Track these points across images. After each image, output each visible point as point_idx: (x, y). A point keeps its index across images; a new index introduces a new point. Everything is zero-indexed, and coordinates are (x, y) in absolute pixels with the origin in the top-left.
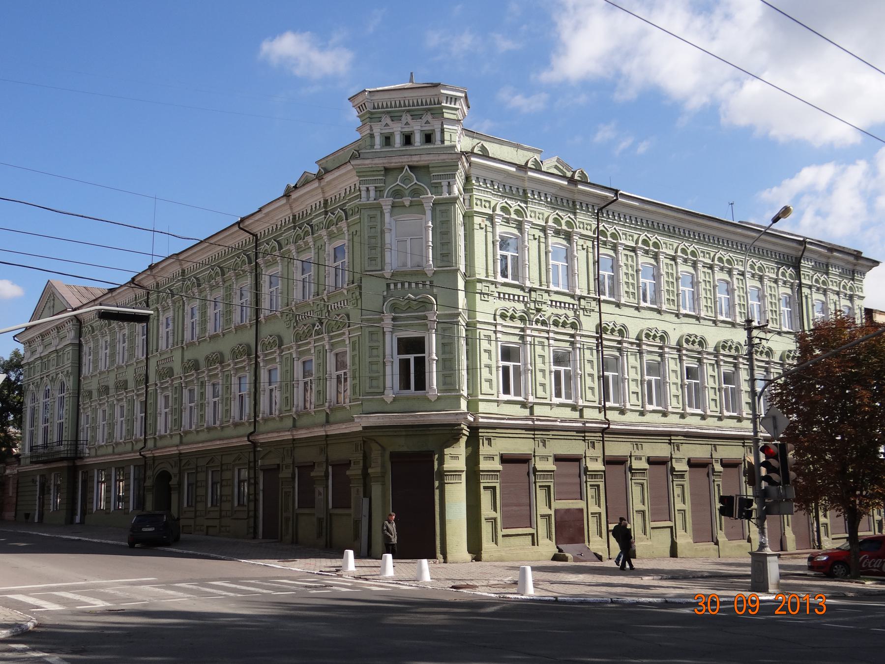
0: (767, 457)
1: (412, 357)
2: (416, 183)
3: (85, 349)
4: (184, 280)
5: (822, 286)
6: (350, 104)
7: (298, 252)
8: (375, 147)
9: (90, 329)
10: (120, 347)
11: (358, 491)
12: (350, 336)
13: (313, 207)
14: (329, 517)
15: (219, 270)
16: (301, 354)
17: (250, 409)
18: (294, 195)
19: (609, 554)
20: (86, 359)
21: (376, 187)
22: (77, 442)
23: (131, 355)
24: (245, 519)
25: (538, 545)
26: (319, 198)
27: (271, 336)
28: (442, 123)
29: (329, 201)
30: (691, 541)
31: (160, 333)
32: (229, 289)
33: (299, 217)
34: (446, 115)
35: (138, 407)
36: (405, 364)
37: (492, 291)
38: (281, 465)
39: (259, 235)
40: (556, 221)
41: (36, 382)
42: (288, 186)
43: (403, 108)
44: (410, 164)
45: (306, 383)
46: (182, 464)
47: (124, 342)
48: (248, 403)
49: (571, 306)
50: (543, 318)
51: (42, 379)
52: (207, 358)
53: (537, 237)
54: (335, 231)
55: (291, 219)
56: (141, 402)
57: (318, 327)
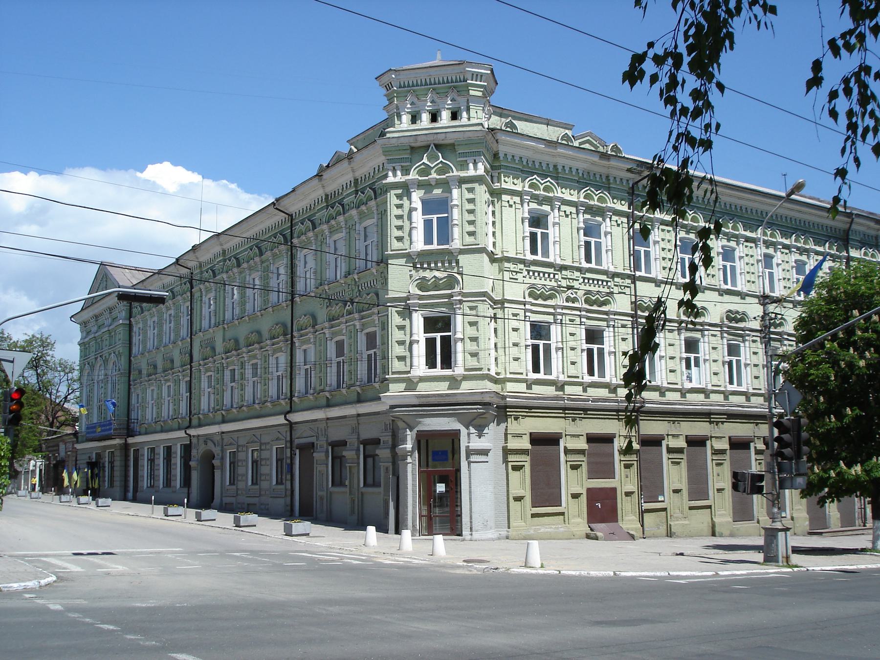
0: (780, 433)
1: (438, 336)
2: (441, 161)
3: (135, 329)
6: (377, 83)
7: (361, 218)
9: (139, 309)
10: (166, 327)
11: (387, 469)
12: (379, 315)
13: (376, 170)
14: (360, 496)
15: (257, 250)
16: (334, 334)
17: (286, 389)
18: (326, 175)
19: (643, 533)
20: (135, 339)
21: (402, 167)
23: (177, 334)
24: (283, 497)
25: (533, 516)
26: (349, 177)
27: (305, 316)
28: (468, 100)
29: (359, 180)
30: (731, 520)
31: (203, 313)
32: (266, 270)
33: (331, 197)
34: (472, 93)
35: (183, 387)
36: (430, 343)
37: (520, 269)
38: (315, 444)
39: (294, 215)
41: (91, 361)
42: (321, 166)
43: (429, 86)
44: (436, 142)
45: (339, 363)
47: (139, 335)
48: (286, 383)
49: (605, 283)
50: (575, 295)
51: (96, 359)
53: (568, 213)
54: (366, 211)
55: (323, 198)
56: (186, 382)
57: (349, 306)
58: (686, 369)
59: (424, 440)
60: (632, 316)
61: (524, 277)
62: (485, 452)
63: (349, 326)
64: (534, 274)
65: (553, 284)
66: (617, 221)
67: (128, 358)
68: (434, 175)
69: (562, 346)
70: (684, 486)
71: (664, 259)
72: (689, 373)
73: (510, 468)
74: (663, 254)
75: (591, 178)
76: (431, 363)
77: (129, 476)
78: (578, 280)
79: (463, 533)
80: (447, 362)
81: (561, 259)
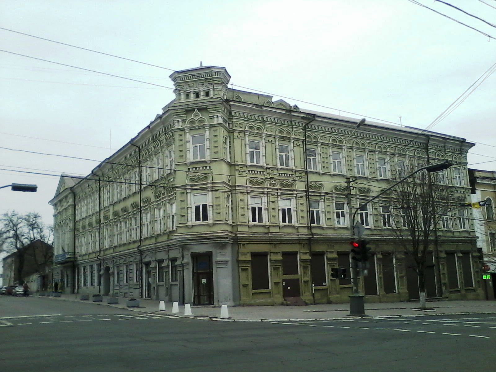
1: (340, 211)
4: (113, 171)
5: (442, 158)
8: (181, 100)
22: (75, 253)
24: (138, 289)
28: (213, 86)
37: (244, 170)
40: (280, 132)
46: (114, 263)
49: (291, 175)
52: (122, 209)
58: (337, 217)
59: (195, 257)
60: (306, 192)
61: (246, 174)
62: (226, 262)
63: (163, 201)
64: (252, 172)
65: (263, 177)
66: (297, 144)
67: (74, 221)
68: (197, 124)
69: (267, 208)
70: (250, 283)
71: (323, 162)
72: (339, 220)
73: (240, 269)
74: (323, 160)
75: (323, 130)
76: (198, 219)
77: (75, 281)
78: (276, 174)
79: (215, 304)
80: (205, 218)
81: (266, 164)
